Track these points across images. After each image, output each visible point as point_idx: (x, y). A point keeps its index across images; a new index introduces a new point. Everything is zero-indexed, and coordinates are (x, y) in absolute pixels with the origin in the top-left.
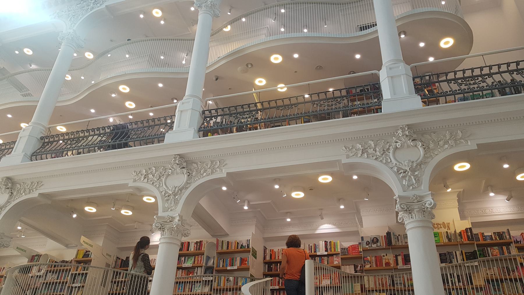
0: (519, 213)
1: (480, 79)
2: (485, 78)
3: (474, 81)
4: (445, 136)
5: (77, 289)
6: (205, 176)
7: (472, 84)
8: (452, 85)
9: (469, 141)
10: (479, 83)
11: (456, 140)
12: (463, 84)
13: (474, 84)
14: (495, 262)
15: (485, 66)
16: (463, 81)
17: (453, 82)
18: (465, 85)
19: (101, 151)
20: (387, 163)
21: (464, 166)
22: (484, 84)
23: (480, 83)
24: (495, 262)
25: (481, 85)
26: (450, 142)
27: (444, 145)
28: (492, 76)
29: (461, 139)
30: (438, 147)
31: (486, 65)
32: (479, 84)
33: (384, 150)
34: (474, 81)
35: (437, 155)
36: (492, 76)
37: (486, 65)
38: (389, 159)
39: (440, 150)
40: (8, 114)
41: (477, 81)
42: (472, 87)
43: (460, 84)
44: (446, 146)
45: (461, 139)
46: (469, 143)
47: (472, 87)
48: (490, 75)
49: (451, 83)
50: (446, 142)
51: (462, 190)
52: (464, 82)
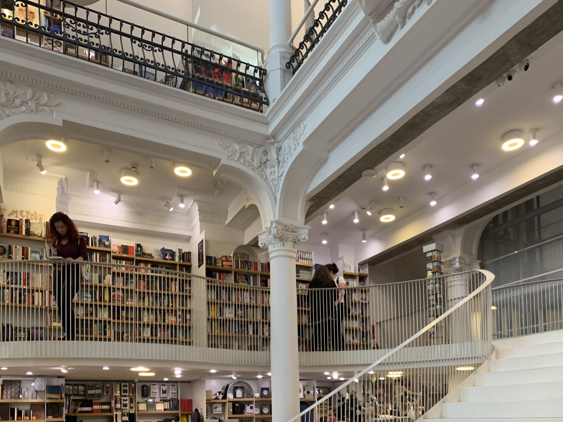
0: (134, 222)
1: (95, 30)
2: (101, 32)
3: (85, 30)
4: (25, 94)
5: (476, 297)
6: (25, 112)
7: (82, 32)
8: (135, 46)
9: (54, 113)
10: (91, 35)
11: (38, 104)
12: (70, 27)
13: (85, 34)
14: (31, 266)
15: (105, 14)
16: (73, 22)
17: (138, 42)
18: (72, 30)
19: (65, 52)
20: (261, 176)
21: (185, 172)
22: (96, 40)
23: (92, 37)
24: (31, 266)
25: (91, 40)
26: (29, 104)
27: (21, 105)
28: (110, 34)
29: (46, 105)
30: (12, 105)
31: (188, 41)
32: (90, 36)
33: (261, 163)
34: (85, 30)
35: (8, 116)
36: (110, 34)
37: (188, 41)
38: (265, 175)
39: (14, 111)
40: (484, 103)
41: (90, 31)
42: (79, 36)
43: (68, 24)
44: (23, 108)
45: (46, 105)
46: (54, 115)
47: (79, 36)
48: (109, 31)
49: (135, 43)
50: (23, 103)
51: (64, 177)
52: (73, 24)
